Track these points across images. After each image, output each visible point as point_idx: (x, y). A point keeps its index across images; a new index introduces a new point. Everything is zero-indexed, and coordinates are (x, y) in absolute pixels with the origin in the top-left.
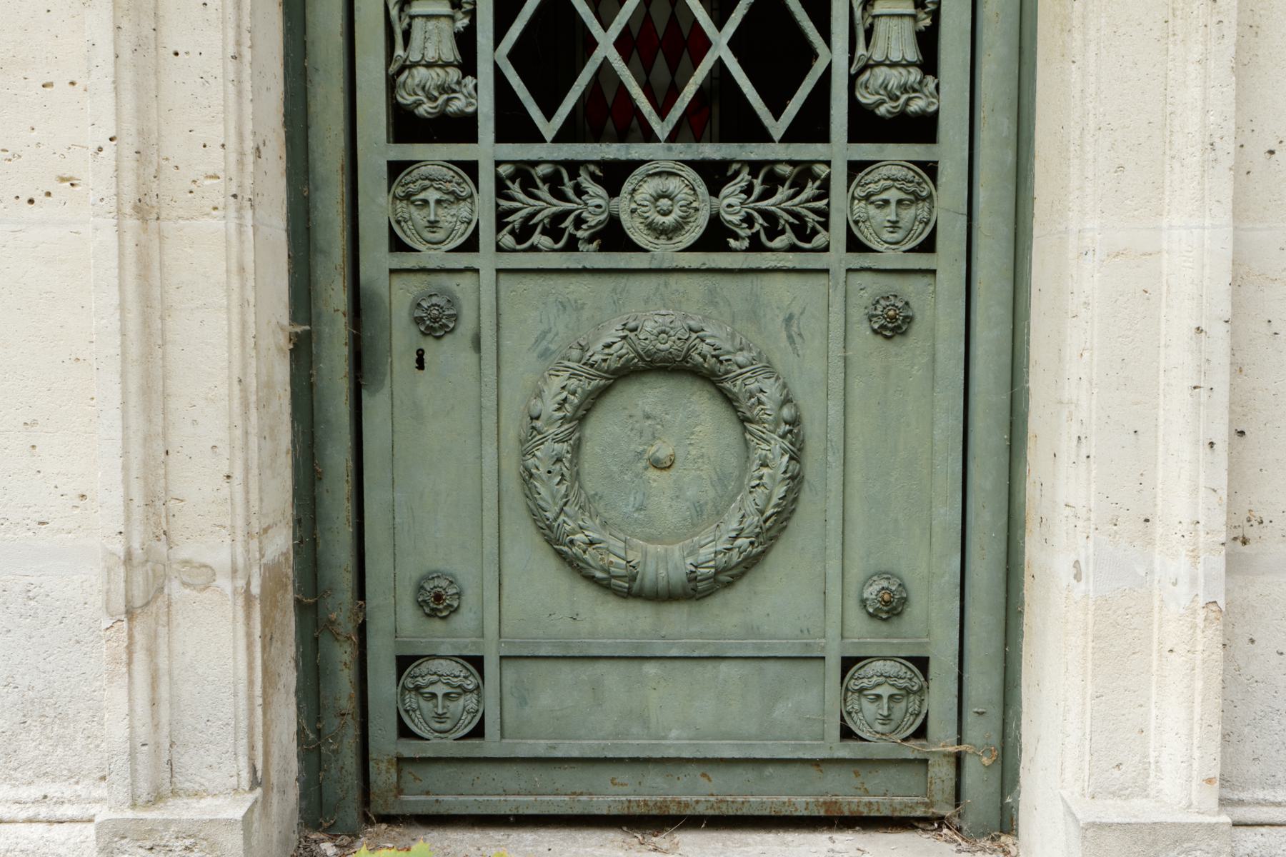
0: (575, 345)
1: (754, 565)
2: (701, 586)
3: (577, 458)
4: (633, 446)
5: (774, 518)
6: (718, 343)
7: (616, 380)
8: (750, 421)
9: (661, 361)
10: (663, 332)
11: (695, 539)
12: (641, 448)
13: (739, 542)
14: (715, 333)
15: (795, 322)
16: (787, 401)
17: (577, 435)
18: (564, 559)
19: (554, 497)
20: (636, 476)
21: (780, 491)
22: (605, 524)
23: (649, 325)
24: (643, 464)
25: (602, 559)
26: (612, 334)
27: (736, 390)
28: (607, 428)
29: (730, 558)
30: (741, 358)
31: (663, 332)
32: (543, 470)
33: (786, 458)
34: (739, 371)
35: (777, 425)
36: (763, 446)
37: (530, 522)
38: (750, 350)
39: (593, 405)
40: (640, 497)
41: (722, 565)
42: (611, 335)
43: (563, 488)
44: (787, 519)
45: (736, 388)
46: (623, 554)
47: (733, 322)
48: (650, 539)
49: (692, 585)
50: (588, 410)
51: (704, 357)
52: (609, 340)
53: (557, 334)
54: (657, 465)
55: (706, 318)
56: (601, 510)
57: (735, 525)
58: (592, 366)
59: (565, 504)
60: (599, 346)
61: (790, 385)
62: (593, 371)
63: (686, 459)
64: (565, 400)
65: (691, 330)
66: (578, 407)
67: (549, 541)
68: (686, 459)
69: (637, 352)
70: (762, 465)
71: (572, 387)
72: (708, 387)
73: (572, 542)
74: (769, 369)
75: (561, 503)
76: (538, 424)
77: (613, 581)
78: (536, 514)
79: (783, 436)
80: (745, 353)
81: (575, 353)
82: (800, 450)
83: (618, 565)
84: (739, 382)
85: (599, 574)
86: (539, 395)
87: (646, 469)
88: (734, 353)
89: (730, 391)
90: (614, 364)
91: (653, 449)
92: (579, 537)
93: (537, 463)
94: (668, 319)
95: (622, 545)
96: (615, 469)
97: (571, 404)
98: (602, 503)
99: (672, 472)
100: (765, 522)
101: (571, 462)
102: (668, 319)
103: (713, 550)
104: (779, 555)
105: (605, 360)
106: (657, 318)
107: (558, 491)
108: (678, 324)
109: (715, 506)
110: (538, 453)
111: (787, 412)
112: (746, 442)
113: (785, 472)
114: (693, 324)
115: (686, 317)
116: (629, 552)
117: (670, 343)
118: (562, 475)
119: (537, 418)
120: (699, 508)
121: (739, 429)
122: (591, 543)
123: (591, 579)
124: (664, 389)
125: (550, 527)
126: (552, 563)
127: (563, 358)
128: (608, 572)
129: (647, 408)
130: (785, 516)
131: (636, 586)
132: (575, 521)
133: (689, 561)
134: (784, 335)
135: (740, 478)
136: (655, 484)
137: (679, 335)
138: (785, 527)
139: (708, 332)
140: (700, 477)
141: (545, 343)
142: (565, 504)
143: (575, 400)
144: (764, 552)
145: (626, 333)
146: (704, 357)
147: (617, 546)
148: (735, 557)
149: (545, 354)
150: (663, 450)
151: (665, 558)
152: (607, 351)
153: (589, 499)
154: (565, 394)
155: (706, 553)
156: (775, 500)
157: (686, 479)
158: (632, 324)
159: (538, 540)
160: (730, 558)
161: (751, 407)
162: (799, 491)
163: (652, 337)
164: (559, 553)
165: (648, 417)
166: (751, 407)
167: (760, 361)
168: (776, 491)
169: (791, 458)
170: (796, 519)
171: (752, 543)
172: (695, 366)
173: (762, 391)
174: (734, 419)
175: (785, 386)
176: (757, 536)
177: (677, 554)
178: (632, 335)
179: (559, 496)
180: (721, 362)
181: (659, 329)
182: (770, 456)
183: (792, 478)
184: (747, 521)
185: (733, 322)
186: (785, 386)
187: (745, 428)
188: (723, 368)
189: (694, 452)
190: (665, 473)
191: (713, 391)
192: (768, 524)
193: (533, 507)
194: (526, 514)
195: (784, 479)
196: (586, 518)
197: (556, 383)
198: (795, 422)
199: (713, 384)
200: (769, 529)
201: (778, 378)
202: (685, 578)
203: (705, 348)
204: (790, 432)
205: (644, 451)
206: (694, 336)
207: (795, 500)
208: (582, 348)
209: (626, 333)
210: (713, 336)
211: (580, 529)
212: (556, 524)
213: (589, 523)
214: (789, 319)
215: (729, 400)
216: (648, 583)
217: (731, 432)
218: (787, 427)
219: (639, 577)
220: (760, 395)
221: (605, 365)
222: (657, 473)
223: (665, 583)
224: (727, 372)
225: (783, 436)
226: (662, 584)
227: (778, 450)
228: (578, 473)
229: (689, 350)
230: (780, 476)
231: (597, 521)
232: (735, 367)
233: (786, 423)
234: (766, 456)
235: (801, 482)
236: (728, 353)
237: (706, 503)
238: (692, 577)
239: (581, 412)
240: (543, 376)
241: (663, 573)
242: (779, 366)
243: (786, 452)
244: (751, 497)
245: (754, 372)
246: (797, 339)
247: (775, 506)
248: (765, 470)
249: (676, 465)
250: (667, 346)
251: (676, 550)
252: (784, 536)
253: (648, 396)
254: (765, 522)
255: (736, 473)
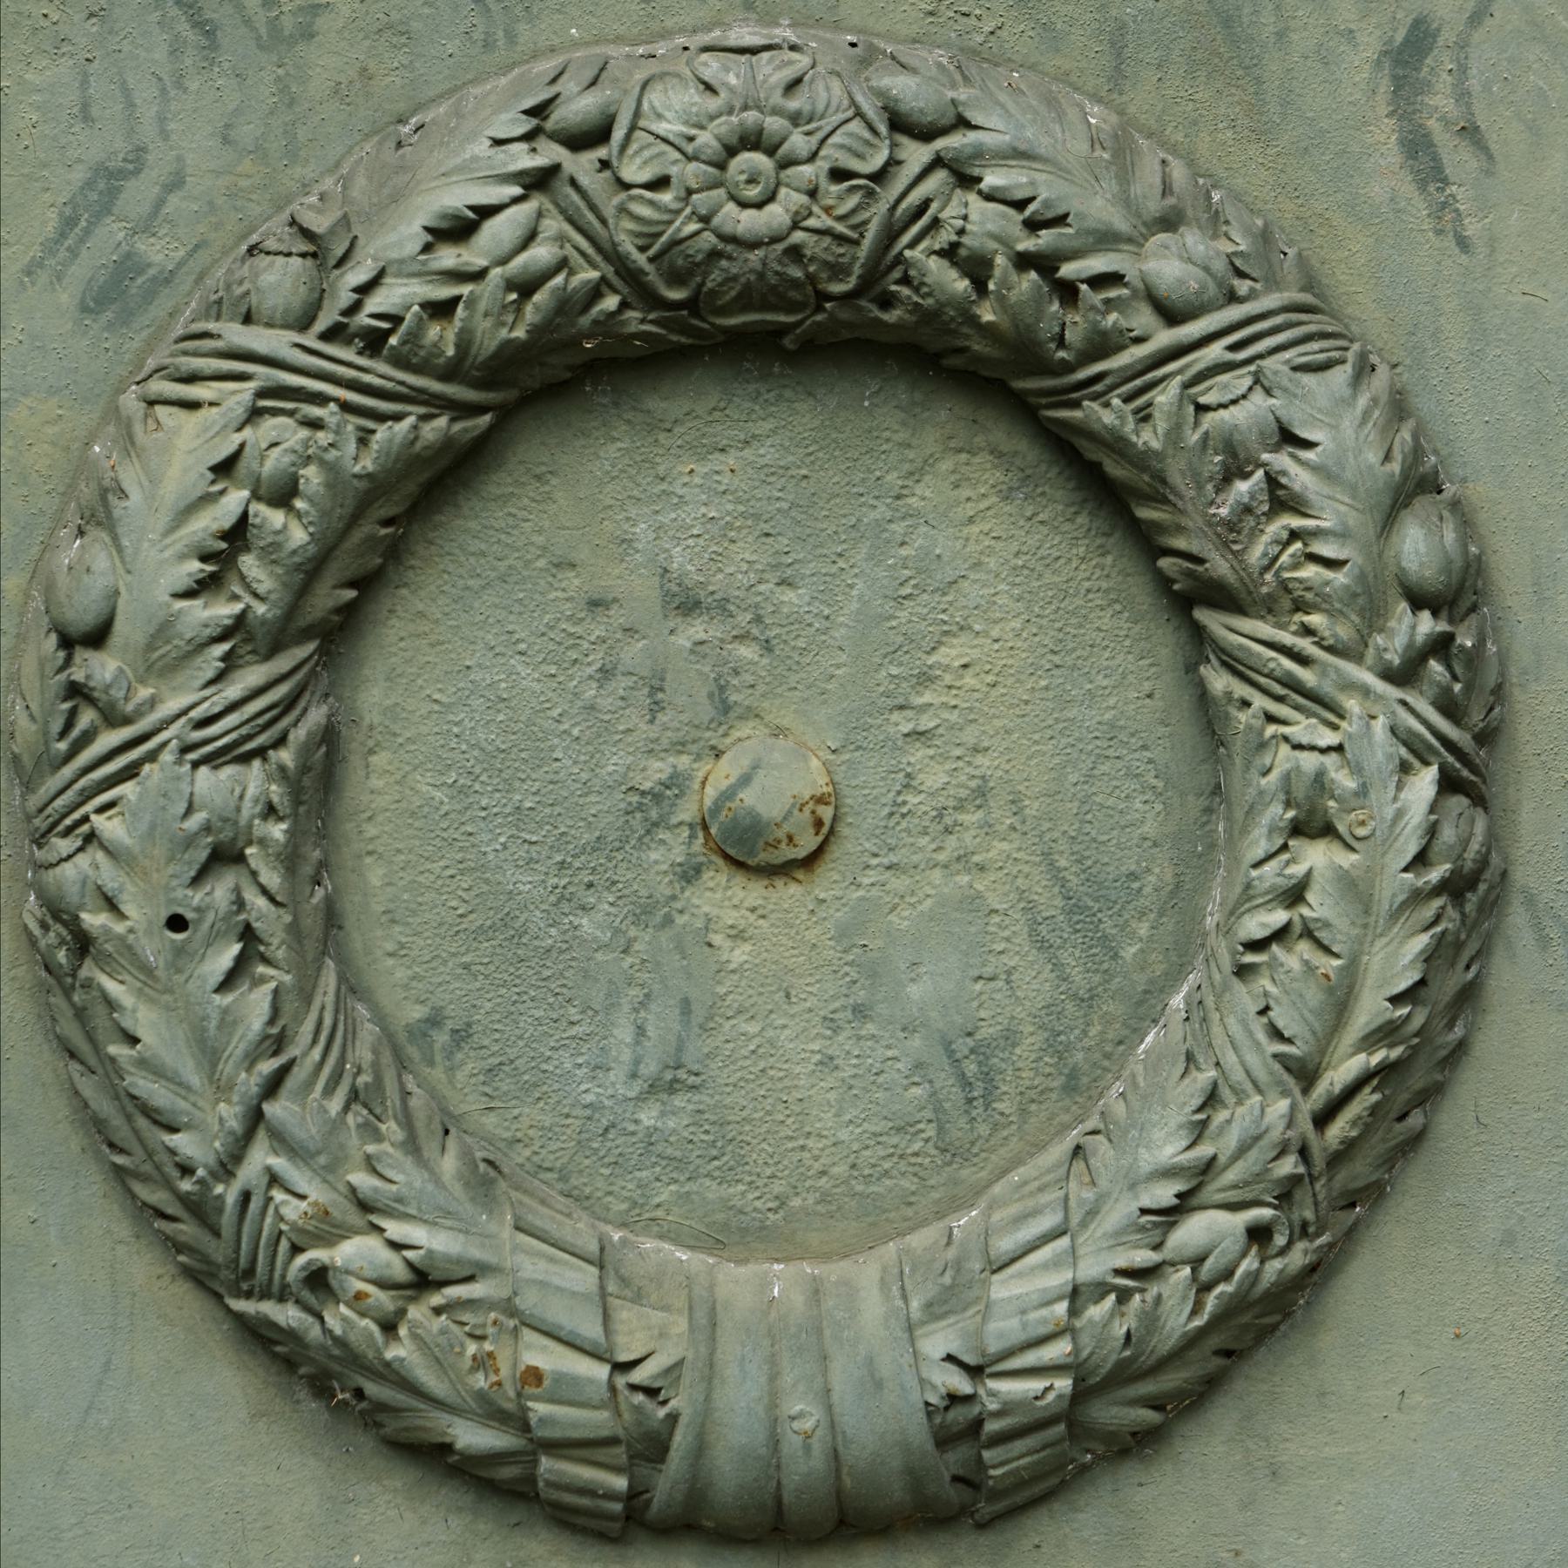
0: (275, 232)
1: (1264, 1334)
2: (1002, 1463)
3: (323, 835)
4: (614, 763)
5: (1367, 1098)
6: (1048, 190)
7: (506, 415)
8: (1227, 599)
9: (746, 300)
10: (752, 140)
11: (962, 1222)
12: (657, 770)
13: (1194, 1231)
14: (1031, 135)
15: (1441, 61)
16: (1417, 485)
17: (316, 716)
18: (289, 1364)
19: (210, 1055)
20: (643, 913)
21: (1399, 958)
22: (486, 1177)
23: (672, 106)
24: (673, 848)
25: (483, 1362)
26: (471, 163)
27: (1149, 438)
28: (477, 676)
29: (1151, 1319)
30: (1169, 265)
31: (752, 140)
32: (140, 915)
33: (1425, 782)
34: (1165, 337)
35: (1373, 617)
36: (1304, 728)
37: (93, 1184)
38: (1215, 223)
39: (395, 552)
40: (662, 1022)
41: (1112, 1353)
42: (468, 171)
43: (255, 1005)
44: (1430, 1095)
45: (1152, 426)
46: (591, 1330)
47: (1118, 76)
48: (728, 1237)
49: (956, 1458)
50: (367, 584)
51: (977, 270)
52: (459, 197)
53: (175, 183)
54: (748, 851)
55: (972, 60)
56: (468, 1103)
57: (1170, 1149)
58: (374, 342)
59: (273, 1086)
60: (406, 235)
61: (1423, 404)
62: (380, 372)
63: (897, 811)
64: (238, 533)
65: (901, 124)
66: (310, 571)
67: (201, 1276)
68: (897, 811)
69: (612, 255)
70: (1297, 829)
71: (275, 462)
72: (1003, 434)
73: (319, 1278)
74: (1318, 324)
75: (249, 1084)
76: (100, 668)
77: (547, 1465)
78: (121, 1137)
79: (1404, 675)
80: (1192, 239)
81: (281, 280)
82: (1485, 738)
83: (565, 1391)
84: (1164, 398)
85: (471, 1436)
86: (98, 513)
87: (689, 874)
88: (1135, 241)
89: (1117, 445)
90: (492, 326)
91: (723, 774)
92: (355, 1253)
93: (110, 876)
94: (772, 71)
95: (584, 1278)
96: (526, 883)
97: (270, 553)
98: (470, 1065)
99: (827, 882)
100: (1323, 1119)
101: (289, 859)
102: (772, 71)
103: (1060, 1279)
104: (1397, 1284)
105: (441, 310)
106: (711, 66)
107: (228, 1020)
108: (825, 93)
109: (1056, 1047)
110: (109, 826)
111: (1419, 546)
112: (1208, 715)
113: (1421, 860)
114: (910, 90)
115: (866, 57)
116: (625, 1314)
117: (789, 199)
118: (248, 934)
119: (98, 637)
120: (973, 1068)
121: (1166, 642)
122: (423, 1280)
123: (433, 1457)
124: (766, 453)
125: (200, 1209)
126: (227, 1384)
127: (216, 309)
128: (518, 1421)
129: (680, 560)
130: (1418, 1079)
131: (667, 1483)
132: (329, 1173)
133: (938, 1342)
134: (1385, 136)
135: (1181, 899)
136: (740, 955)
137: (833, 155)
138: (1416, 1140)
139: (996, 127)
140: (972, 901)
141: (112, 232)
142: (273, 1086)
143: (293, 531)
144: (1316, 1274)
145: (549, 153)
146: (977, 270)
147: (558, 1283)
148: (1176, 1311)
149: (116, 293)
150: (773, 777)
151: (815, 1336)
152: (448, 257)
153: (398, 1050)
154: (235, 500)
155: (1023, 1297)
156: (1371, 1009)
157: (901, 921)
158: (578, 107)
159: (145, 1270)
160: (1151, 1319)
161: (1232, 530)
162: (1482, 953)
163: (693, 172)
164: (260, 1338)
165: (687, 605)
166: (1232, 530)
167: (1273, 283)
168: (1374, 961)
169: (1448, 784)
170: (1472, 1090)
171: (1258, 1235)
172: (929, 317)
173: (1288, 438)
174: (1140, 591)
175: (1399, 407)
176: (1286, 1194)
177: (873, 1308)
178: (581, 166)
179: (238, 1046)
180: (1067, 292)
181: (726, 126)
182: (1345, 781)
183: (1455, 888)
184: (1234, 1123)
185: (1118, 76)
186: (1399, 407)
187: (1199, 634)
188: (1077, 327)
189: (934, 778)
190: (789, 893)
191: (1026, 449)
192: (1338, 1129)
193: (104, 1106)
194: (72, 1142)
195: (1418, 897)
196: (387, 1149)
197: (187, 443)
198: (1456, 595)
199: (1025, 411)
200: (1337, 1159)
201: (1364, 369)
202: (918, 1431)
203: (982, 221)
204: (1441, 646)
205: (676, 783)
206: (916, 155)
207: (1468, 996)
208: (314, 247)
209: (549, 153)
210: (1018, 155)
211: (369, 1220)
212: (229, 1194)
213: (404, 1176)
214: (1409, 54)
215: (1111, 491)
216: (728, 1472)
217: (1126, 662)
218: (1426, 625)
219: (680, 1440)
220: (1281, 460)
221: (442, 337)
222: (752, 892)
223: (818, 1461)
224: (1103, 345)
225: (1404, 675)
226: (803, 1467)
227: (1381, 747)
228: (332, 917)
229: (891, 234)
230: (1395, 882)
231: (449, 1164)
232: (1143, 318)
233: (1418, 600)
234: (1319, 780)
235: (1493, 906)
236: (1106, 239)
237: (1010, 1037)
238: (957, 1426)
239: (328, 597)
240: (113, 412)
241: (802, 1412)
242: (1363, 305)
243: (1422, 754)
244: (1245, 998)
245: (1242, 336)
246: (1457, 158)
247: (1370, 1041)
248: (1316, 856)
249: (853, 843)
250: (776, 215)
251: (867, 1285)
252: (1414, 1179)
253: (678, 500)
254: (1323, 1119)
255: (1160, 873)
